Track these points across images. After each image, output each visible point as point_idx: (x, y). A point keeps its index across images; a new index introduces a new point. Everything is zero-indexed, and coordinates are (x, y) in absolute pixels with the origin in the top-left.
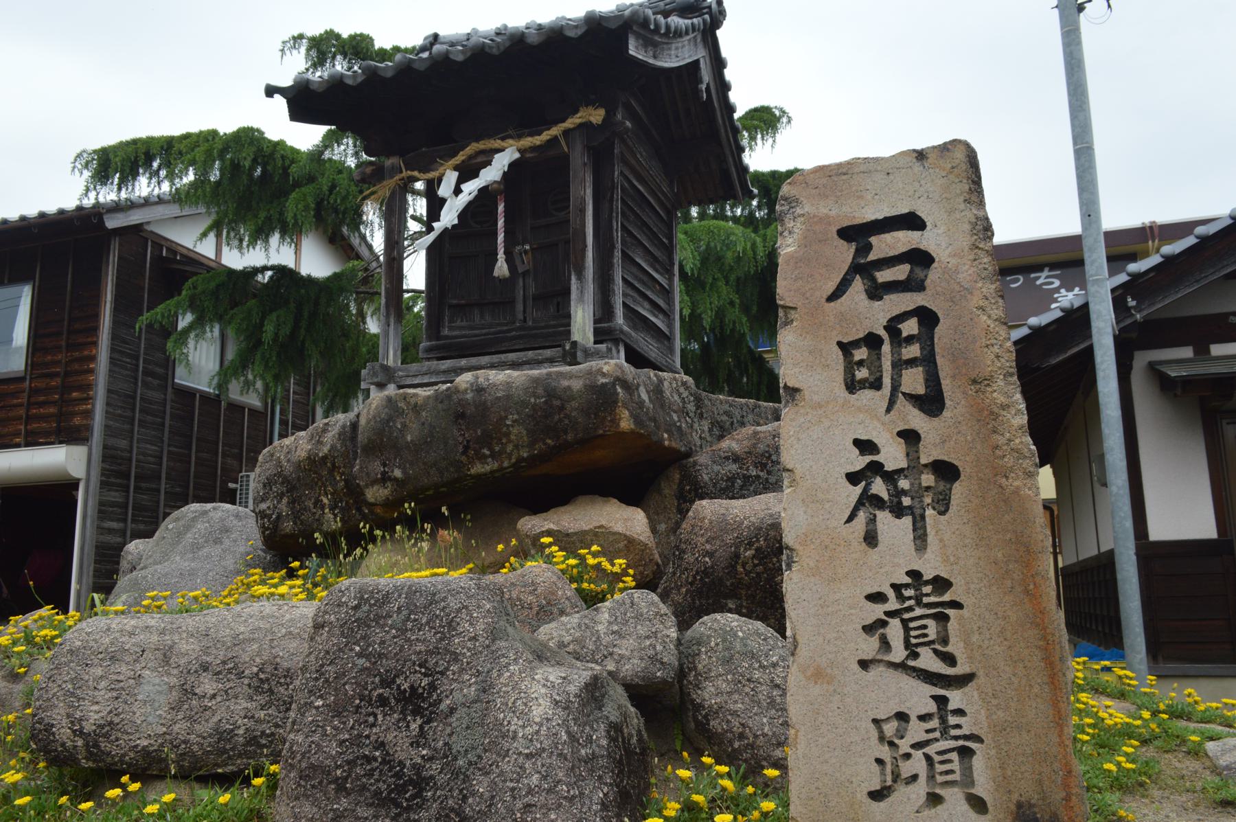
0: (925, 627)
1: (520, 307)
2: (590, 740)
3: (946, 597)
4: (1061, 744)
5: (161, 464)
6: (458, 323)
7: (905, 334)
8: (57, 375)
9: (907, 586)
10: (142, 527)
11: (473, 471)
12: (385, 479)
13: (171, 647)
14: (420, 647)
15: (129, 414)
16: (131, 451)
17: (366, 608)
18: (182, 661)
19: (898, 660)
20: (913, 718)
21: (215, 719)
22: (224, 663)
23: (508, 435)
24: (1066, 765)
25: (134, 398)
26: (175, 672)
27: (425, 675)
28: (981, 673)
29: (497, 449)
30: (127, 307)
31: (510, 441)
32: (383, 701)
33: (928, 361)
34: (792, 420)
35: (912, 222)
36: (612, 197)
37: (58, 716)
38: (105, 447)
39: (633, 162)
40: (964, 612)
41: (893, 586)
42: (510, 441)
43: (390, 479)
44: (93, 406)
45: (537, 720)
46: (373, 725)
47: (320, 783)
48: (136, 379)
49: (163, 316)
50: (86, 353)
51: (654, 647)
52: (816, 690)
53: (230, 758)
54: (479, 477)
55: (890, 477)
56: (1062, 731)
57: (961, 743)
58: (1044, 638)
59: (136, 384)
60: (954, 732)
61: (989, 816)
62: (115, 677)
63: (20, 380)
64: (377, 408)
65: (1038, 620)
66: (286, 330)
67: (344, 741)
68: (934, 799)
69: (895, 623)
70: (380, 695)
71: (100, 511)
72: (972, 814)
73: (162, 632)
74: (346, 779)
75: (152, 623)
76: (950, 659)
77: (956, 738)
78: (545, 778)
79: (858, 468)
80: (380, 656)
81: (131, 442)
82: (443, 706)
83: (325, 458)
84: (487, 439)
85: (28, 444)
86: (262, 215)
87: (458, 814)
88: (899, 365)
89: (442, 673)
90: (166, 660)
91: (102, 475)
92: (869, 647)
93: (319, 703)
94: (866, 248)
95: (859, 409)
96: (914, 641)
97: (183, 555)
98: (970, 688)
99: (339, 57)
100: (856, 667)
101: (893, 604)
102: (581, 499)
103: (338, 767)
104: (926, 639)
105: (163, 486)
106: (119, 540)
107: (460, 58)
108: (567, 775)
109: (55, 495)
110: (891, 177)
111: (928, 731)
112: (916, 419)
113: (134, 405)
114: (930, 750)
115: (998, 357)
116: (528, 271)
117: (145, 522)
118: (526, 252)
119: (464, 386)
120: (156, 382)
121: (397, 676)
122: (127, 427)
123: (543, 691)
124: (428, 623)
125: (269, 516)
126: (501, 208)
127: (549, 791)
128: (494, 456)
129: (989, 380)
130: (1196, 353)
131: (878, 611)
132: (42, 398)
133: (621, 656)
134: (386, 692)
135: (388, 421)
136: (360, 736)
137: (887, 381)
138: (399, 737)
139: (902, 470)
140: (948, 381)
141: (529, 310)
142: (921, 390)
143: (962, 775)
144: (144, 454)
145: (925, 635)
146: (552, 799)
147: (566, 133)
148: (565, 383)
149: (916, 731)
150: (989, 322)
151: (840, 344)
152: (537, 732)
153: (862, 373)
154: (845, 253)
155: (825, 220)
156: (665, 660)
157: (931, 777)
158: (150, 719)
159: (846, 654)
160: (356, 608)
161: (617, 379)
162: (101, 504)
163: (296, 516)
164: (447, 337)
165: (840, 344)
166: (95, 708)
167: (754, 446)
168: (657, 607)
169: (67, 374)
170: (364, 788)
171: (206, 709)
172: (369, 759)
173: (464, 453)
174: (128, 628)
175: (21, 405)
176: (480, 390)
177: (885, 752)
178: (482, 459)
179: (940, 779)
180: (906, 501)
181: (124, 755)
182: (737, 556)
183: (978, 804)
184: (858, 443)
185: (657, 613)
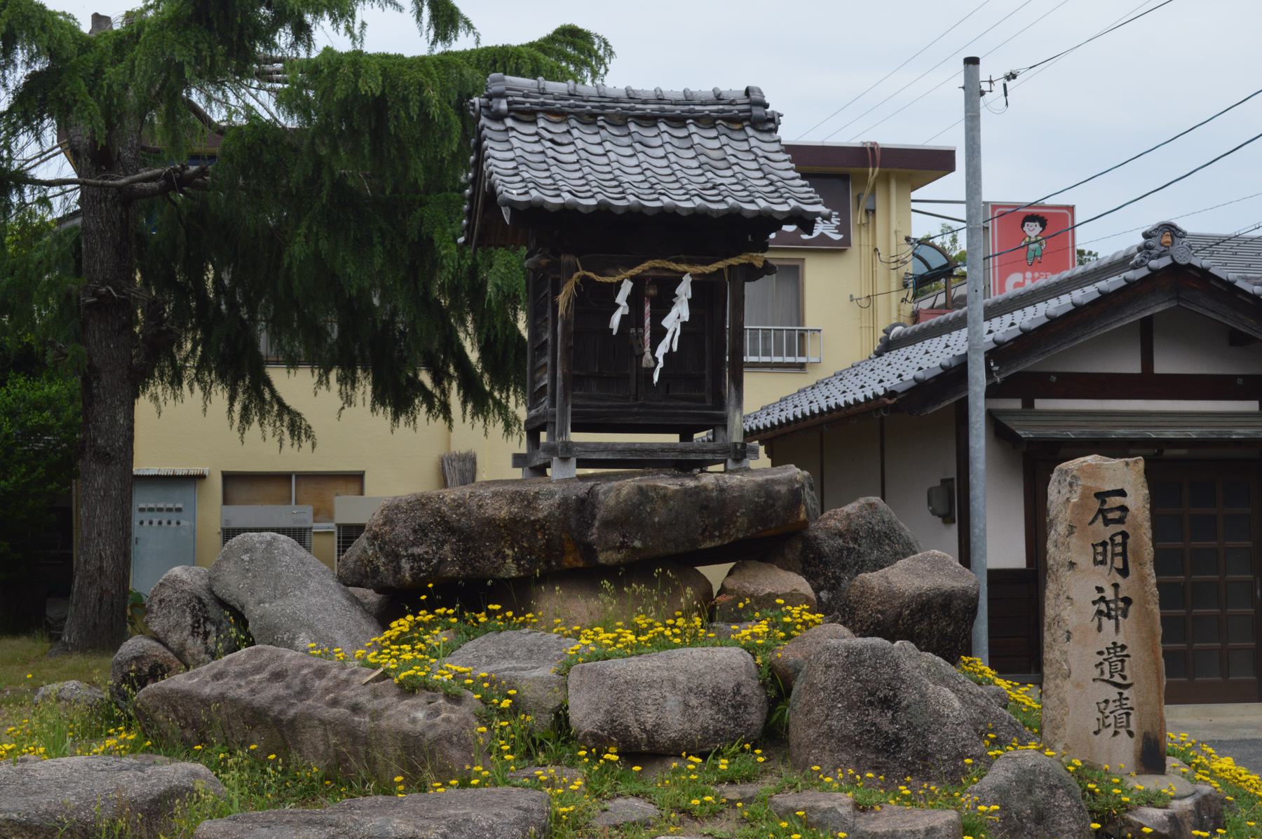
23: (735, 522)
33: (1124, 554)
37: (630, 720)
43: (628, 547)
52: (1077, 691)
55: (1107, 603)
64: (628, 493)
65: (1156, 663)
68: (1116, 733)
76: (1124, 678)
88: (1114, 555)
94: (1104, 502)
101: (1106, 656)
112: (1119, 579)
125: (428, 562)
126: (647, 308)
130: (1024, 405)
131: (1100, 658)
134: (872, 699)
137: (1109, 561)
138: (883, 721)
148: (777, 488)
153: (1100, 558)
167: (849, 525)
170: (869, 745)
172: (869, 731)
173: (702, 534)
176: (722, 490)
177: (1100, 715)
178: (712, 537)
180: (1113, 613)
182: (900, 614)
183: (1130, 734)
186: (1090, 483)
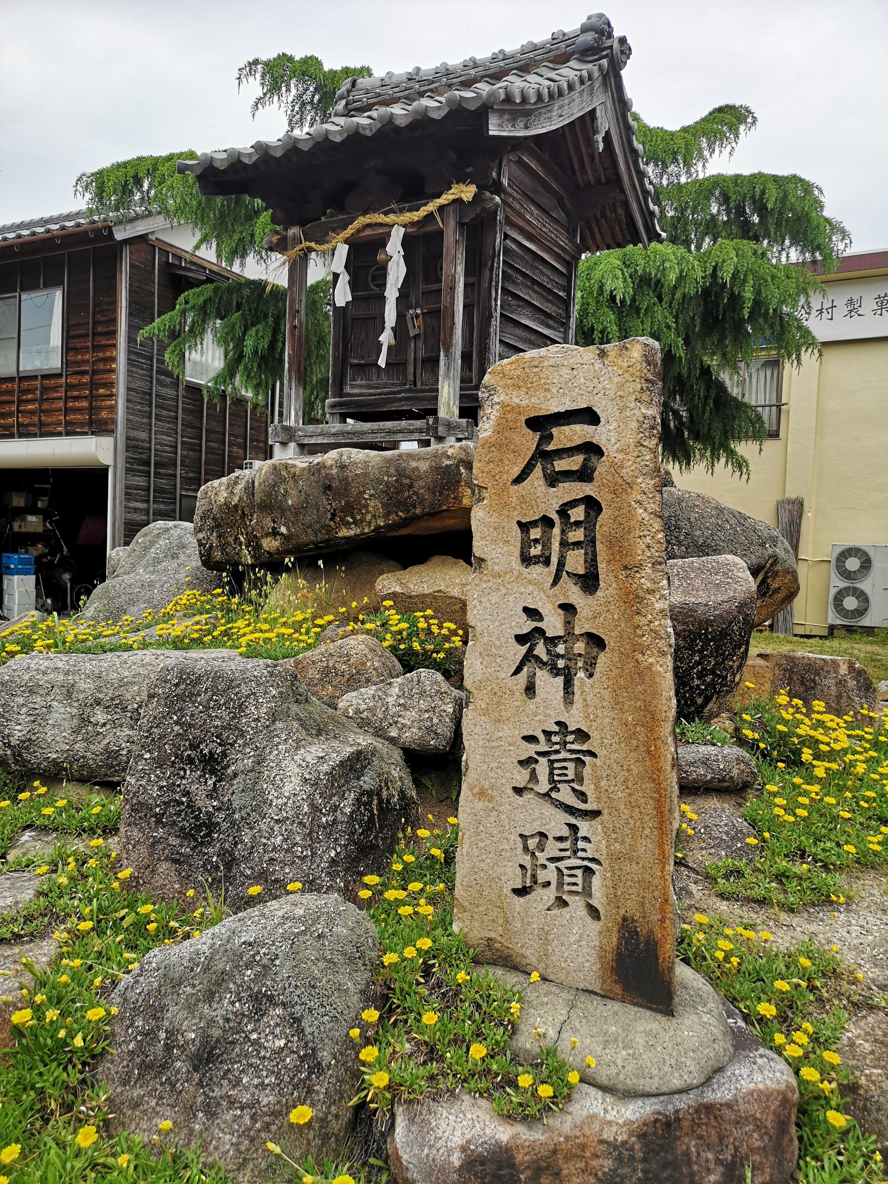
0: (566, 768)
1: (411, 369)
2: (335, 808)
3: (585, 747)
4: (662, 877)
5: (176, 453)
6: (359, 382)
7: (572, 520)
8: (85, 373)
9: (556, 733)
10: (162, 507)
11: (340, 534)
12: (275, 533)
13: (73, 685)
14: (218, 723)
15: (147, 409)
16: (150, 442)
17: (183, 687)
18: (81, 697)
19: (542, 792)
20: (550, 838)
21: (105, 742)
22: (112, 699)
23: (366, 506)
24: (664, 894)
25: (150, 395)
26: (76, 704)
27: (220, 744)
28: (605, 812)
29: (358, 517)
30: (141, 312)
31: (368, 512)
32: (191, 761)
33: (590, 541)
34: (477, 585)
35: (589, 416)
36: (564, 208)
38: (128, 438)
39: (521, 223)
40: (598, 761)
41: (544, 731)
42: (368, 512)
44: (116, 401)
45: (287, 794)
46: (183, 778)
47: (146, 815)
48: (151, 377)
49: (159, 330)
50: (108, 354)
51: (432, 720)
52: (480, 805)
53: (116, 771)
54: (347, 539)
56: (664, 867)
57: (586, 863)
58: (658, 791)
59: (151, 382)
60: (580, 854)
61: (601, 923)
62: (32, 706)
63: (59, 376)
66: (265, 344)
67: (163, 787)
69: (543, 761)
70: (189, 755)
71: (127, 494)
72: (589, 919)
73: (67, 673)
74: (163, 814)
75: (60, 665)
76: (582, 796)
77: (583, 859)
78: (285, 840)
79: (525, 632)
80: (190, 725)
81: (150, 434)
82: (229, 771)
83: (236, 506)
84: (349, 509)
85: (68, 433)
86: (236, 237)
87: (230, 855)
89: (232, 745)
90: (69, 694)
91: (127, 462)
92: (521, 777)
93: (147, 756)
95: (530, 582)
96: (556, 778)
97: (145, 567)
98: (596, 822)
99: (293, 82)
100: (510, 792)
101: (543, 747)
102: (436, 559)
103: (157, 806)
104: (566, 778)
105: (178, 472)
106: (144, 517)
107: (338, 139)
108: (304, 839)
109: (88, 481)
110: (575, 372)
111: (561, 850)
112: (574, 594)
113: (151, 400)
114: (562, 865)
115: (648, 547)
116: (419, 335)
117: (164, 503)
118: (417, 316)
119: (330, 462)
120: (168, 380)
121: (201, 743)
122: (145, 420)
123: (297, 770)
124: (224, 704)
125: (204, 545)
127: (287, 851)
128: (355, 522)
129: (640, 566)
131: (531, 750)
132: (76, 393)
133: (404, 725)
135: (274, 486)
136: (174, 784)
137: (554, 560)
139: (559, 637)
140: (604, 566)
141: (418, 372)
142: (582, 571)
143: (584, 888)
144: (161, 445)
145: (566, 775)
146: (288, 857)
147: (441, 208)
148: (414, 464)
149: (552, 848)
150: (644, 515)
151: (519, 523)
152: (286, 804)
153: (536, 551)
154: (530, 441)
155: (517, 409)
156: (439, 731)
157: (560, 884)
158: (58, 738)
159: (504, 781)
160: (177, 685)
161: (461, 461)
162: (127, 487)
163: (223, 547)
164: (349, 395)
165: (519, 523)
166: (18, 727)
168: (439, 686)
169: (94, 372)
170: (174, 823)
171: (98, 734)
173: (332, 519)
174: (42, 668)
175: (60, 398)
176: (343, 467)
177: (527, 860)
178: (347, 525)
179: (566, 888)
180: (561, 663)
181: (40, 763)
183: (594, 913)
184: (526, 610)
185: (438, 691)
186: (517, 399)
